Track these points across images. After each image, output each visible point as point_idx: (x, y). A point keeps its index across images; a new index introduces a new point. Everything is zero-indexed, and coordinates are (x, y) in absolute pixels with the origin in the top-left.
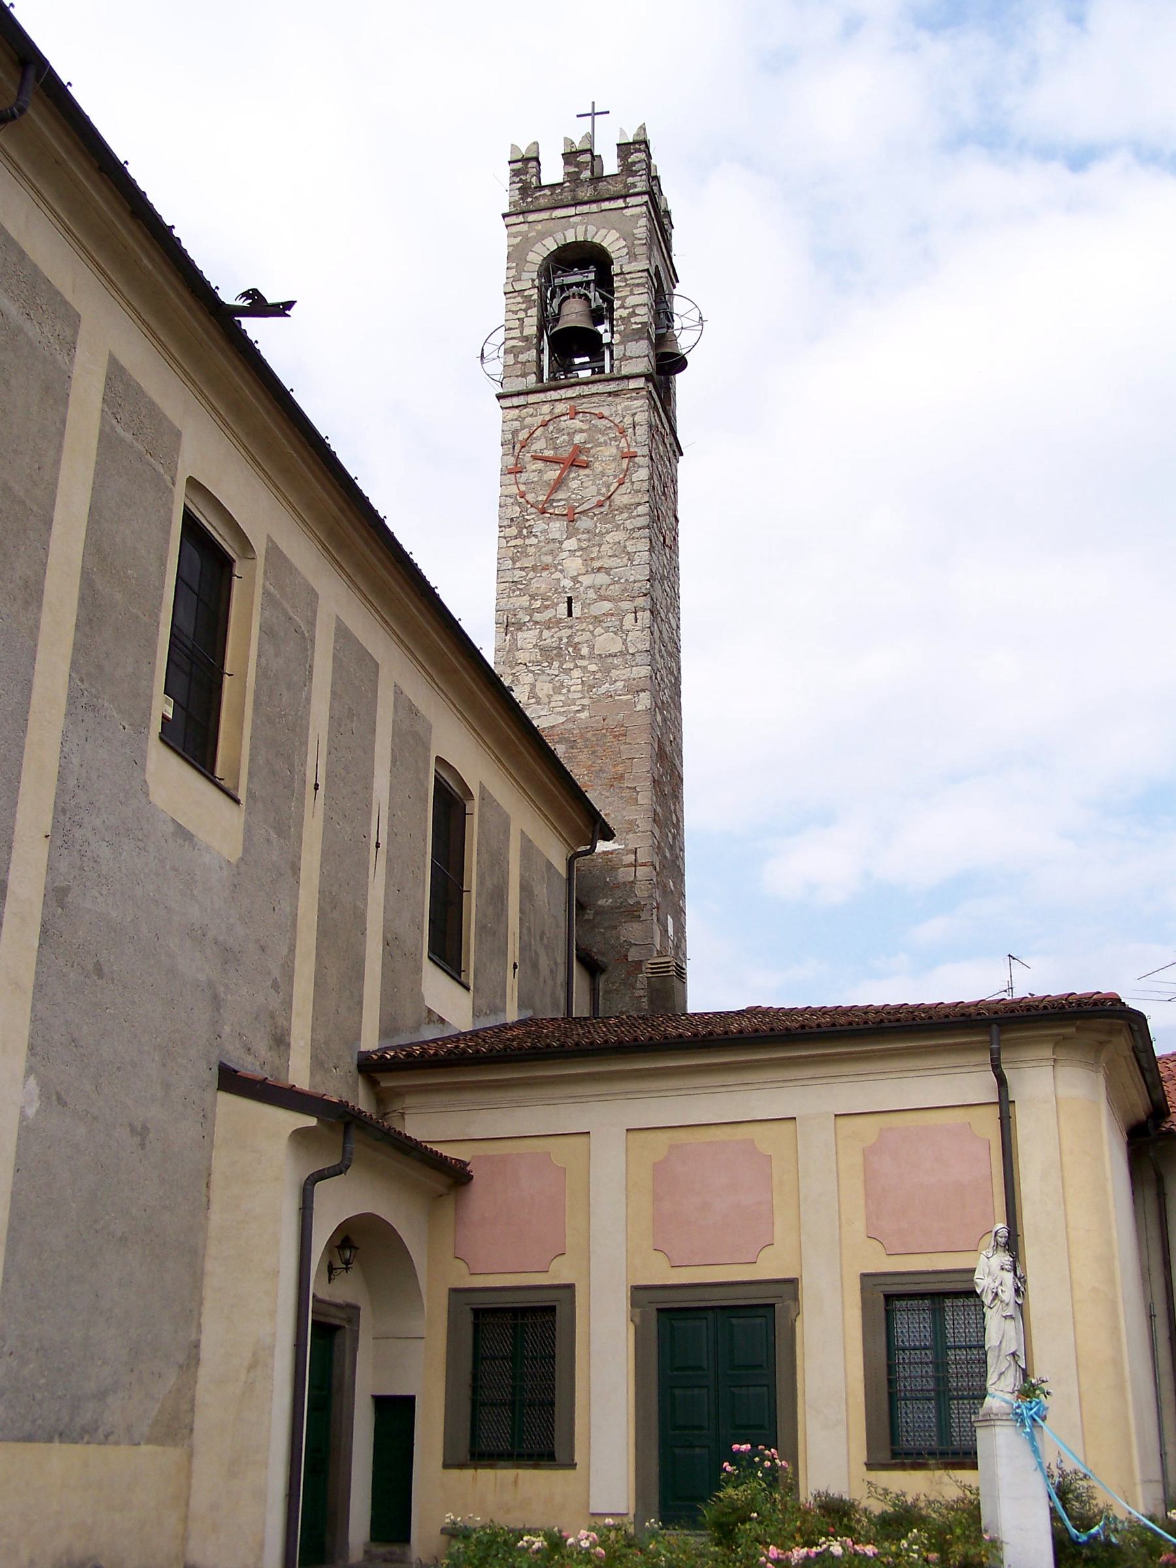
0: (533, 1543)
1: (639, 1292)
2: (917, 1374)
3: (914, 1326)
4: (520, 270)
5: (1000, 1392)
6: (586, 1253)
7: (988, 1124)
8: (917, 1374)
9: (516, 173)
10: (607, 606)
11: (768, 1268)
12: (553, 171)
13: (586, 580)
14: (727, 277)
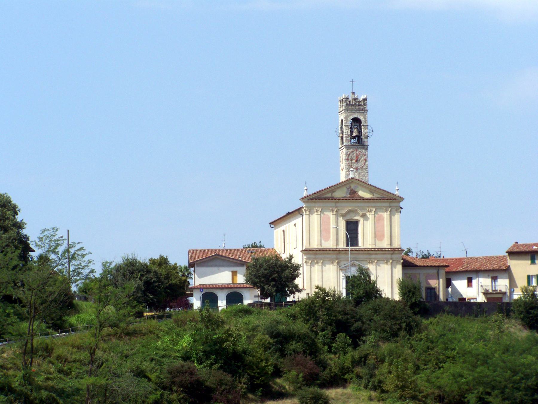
3: (429, 291)
7: (437, 275)
14: (372, 120)
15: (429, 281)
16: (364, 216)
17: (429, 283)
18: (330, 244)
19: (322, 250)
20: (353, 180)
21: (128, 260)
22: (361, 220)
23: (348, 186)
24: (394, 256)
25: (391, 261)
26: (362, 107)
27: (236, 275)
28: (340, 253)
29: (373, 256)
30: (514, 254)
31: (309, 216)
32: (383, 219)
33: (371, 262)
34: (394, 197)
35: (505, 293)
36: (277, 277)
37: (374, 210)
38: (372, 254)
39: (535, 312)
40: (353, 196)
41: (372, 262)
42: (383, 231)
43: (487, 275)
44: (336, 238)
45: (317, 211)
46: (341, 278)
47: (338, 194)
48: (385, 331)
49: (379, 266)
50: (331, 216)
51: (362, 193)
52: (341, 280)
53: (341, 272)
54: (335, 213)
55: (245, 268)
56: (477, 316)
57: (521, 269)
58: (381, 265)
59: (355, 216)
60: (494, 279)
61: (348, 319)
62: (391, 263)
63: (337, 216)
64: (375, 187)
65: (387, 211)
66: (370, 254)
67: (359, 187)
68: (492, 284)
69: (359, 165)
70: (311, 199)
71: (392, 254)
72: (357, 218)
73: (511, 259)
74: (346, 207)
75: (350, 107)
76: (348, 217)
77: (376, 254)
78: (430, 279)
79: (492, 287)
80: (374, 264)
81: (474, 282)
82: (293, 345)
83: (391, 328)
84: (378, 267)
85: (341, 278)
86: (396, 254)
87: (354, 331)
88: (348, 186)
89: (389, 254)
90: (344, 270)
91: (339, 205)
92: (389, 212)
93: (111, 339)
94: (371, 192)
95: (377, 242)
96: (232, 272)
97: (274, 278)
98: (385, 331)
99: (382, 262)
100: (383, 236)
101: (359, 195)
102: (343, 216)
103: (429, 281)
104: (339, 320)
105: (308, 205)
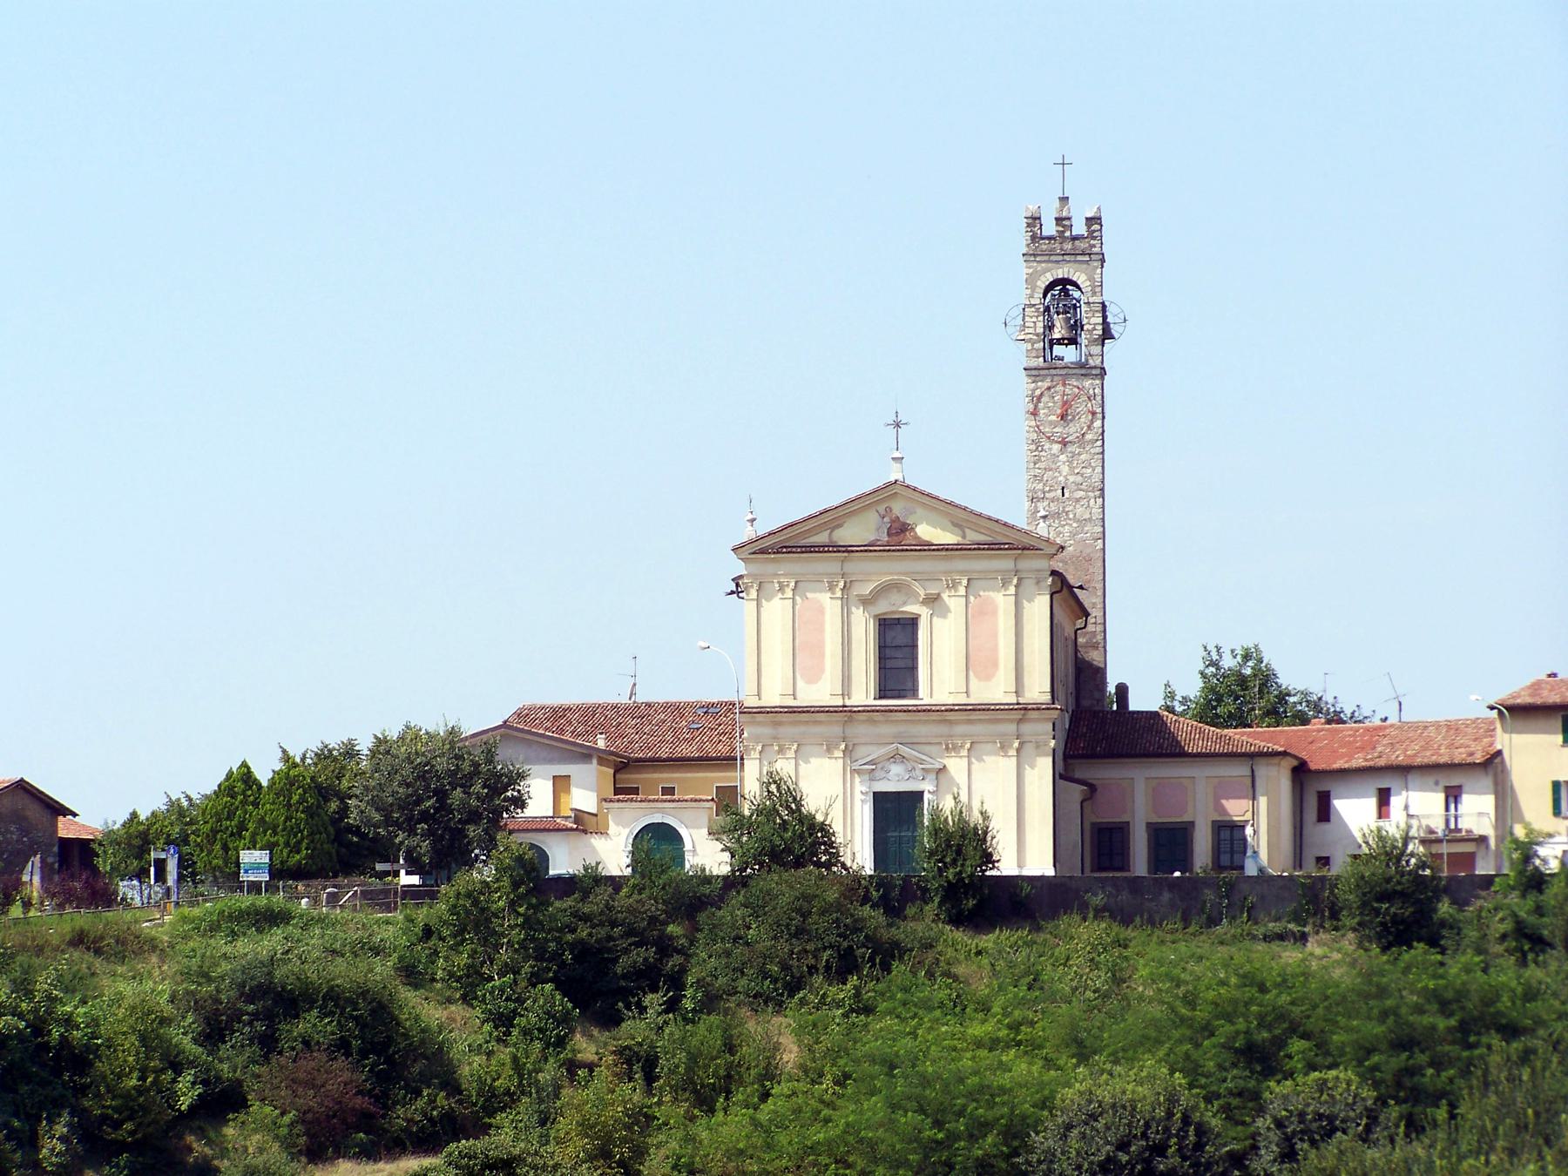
0: (1388, 962)
1: (1149, 825)
2: (1225, 846)
3: (1225, 834)
4: (1033, 290)
5: (1249, 853)
6: (1133, 812)
7: (1249, 782)
8: (1225, 846)
9: (1029, 225)
10: (1081, 494)
11: (1186, 818)
12: (1050, 228)
13: (1071, 479)
14: (1120, 283)
15: (1224, 802)
16: (932, 600)
17: (1224, 811)
18: (821, 692)
19: (792, 710)
20: (897, 489)
21: (453, 732)
22: (923, 612)
23: (882, 509)
24: (1027, 728)
25: (1016, 745)
26: (1081, 245)
27: (568, 791)
28: (851, 720)
29: (960, 729)
30: (1520, 713)
31: (759, 606)
32: (995, 612)
33: (951, 749)
34: (1027, 541)
35: (1483, 840)
36: (433, 806)
37: (965, 582)
38: (957, 722)
39: (1393, 910)
40: (898, 536)
41: (956, 748)
42: (995, 649)
43: (1431, 780)
44: (842, 670)
45: (782, 589)
46: (858, 797)
47: (851, 533)
48: (765, 975)
49: (980, 759)
50: (828, 604)
51: (927, 531)
52: (858, 803)
53: (857, 779)
54: (839, 594)
55: (595, 761)
56: (1213, 921)
57: (1537, 759)
58: (812, 760)
59: (905, 604)
60: (1453, 795)
61: (610, 938)
62: (1018, 750)
63: (846, 602)
64: (965, 509)
65: (1005, 584)
66: (950, 722)
67: (920, 511)
68: (1447, 809)
69: (1073, 430)
70: (763, 551)
71: (1020, 721)
72: (912, 608)
73: (1505, 730)
74: (874, 573)
75: (1044, 245)
76: (883, 607)
77: (970, 722)
78: (1227, 798)
79: (1447, 822)
80: (964, 753)
81: (1396, 802)
82: (310, 1023)
83: (785, 967)
84: (976, 765)
85: (858, 797)
86: (1030, 720)
87: (624, 976)
88: (882, 509)
89: (1011, 721)
90: (872, 770)
91: (856, 566)
92: (1012, 590)
93: (1303, 938)
94: (957, 525)
95: (974, 683)
96: (556, 779)
97: (426, 811)
98: (765, 975)
99: (989, 746)
100: (995, 665)
101: (916, 537)
102: (866, 602)
103: (1224, 802)
104: (581, 941)
105: (755, 568)
